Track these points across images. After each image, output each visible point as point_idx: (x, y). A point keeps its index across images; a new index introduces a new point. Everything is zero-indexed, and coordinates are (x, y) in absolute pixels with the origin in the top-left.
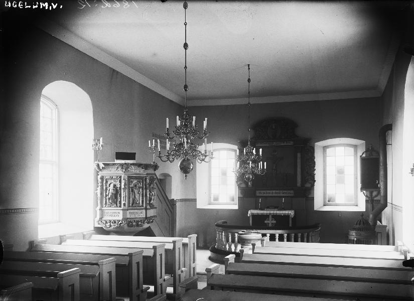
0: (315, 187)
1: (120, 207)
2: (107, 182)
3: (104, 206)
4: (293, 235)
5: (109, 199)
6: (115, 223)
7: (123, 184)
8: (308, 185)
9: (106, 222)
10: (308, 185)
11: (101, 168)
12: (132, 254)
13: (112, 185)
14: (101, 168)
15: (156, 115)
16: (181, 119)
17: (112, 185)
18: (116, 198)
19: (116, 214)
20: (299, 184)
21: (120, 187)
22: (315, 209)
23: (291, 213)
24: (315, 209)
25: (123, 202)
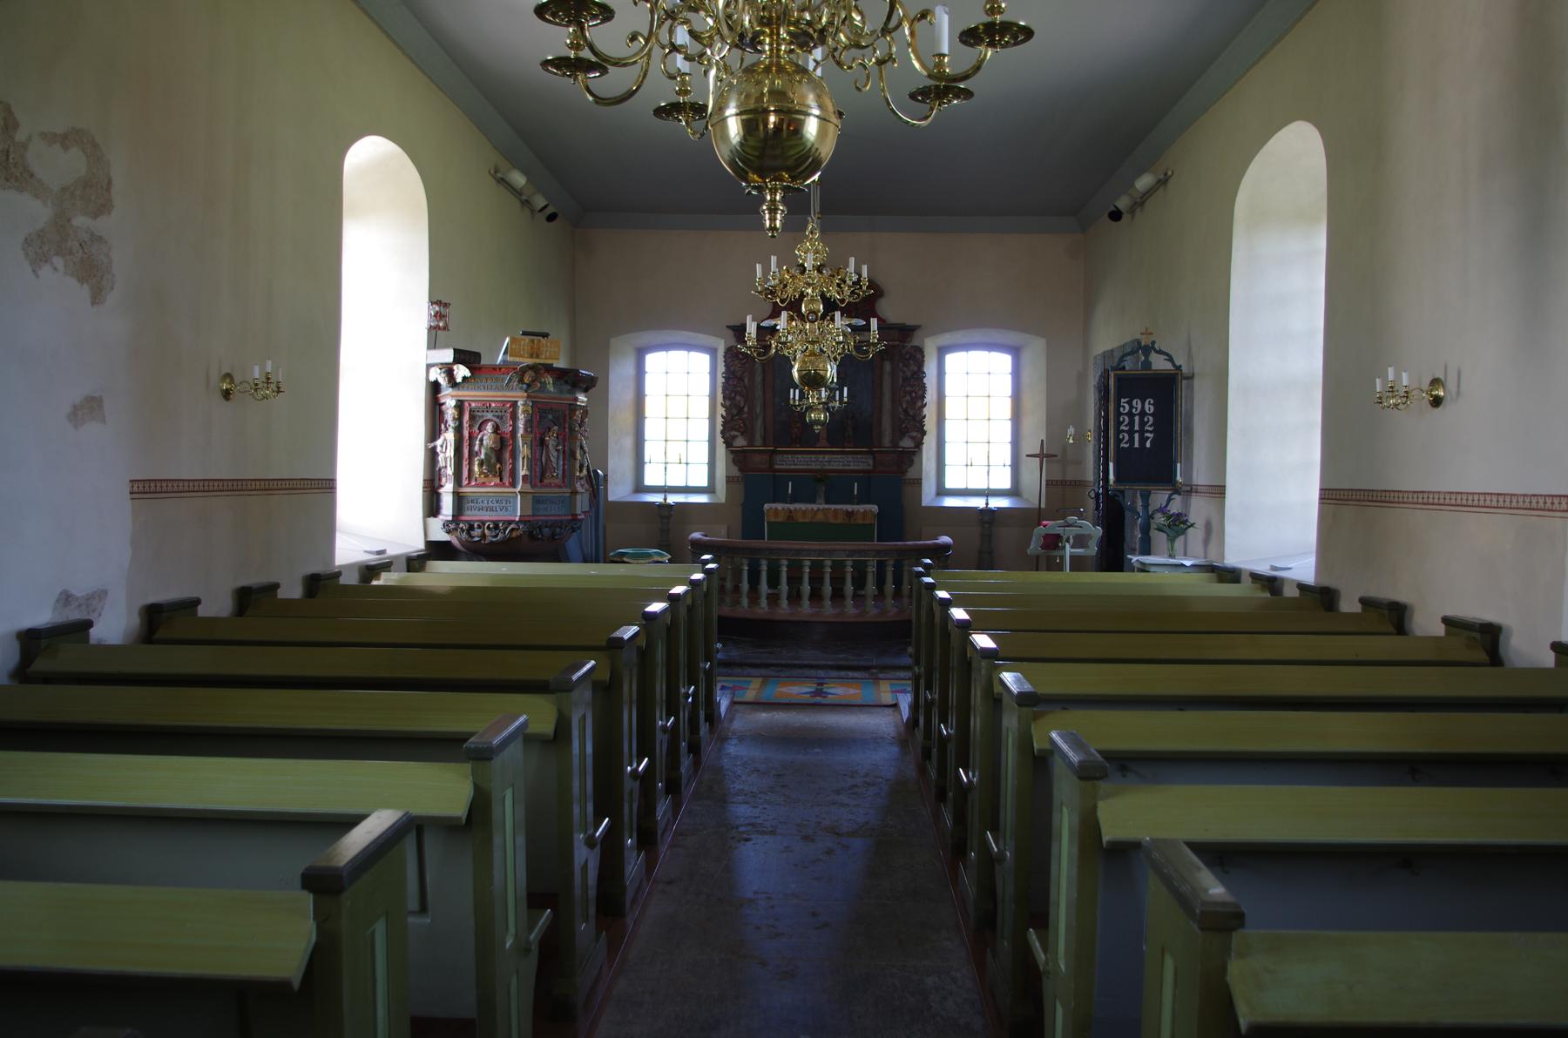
0: (924, 447)
1: (513, 485)
2: (472, 418)
3: (465, 482)
4: (785, 562)
5: (481, 464)
6: (496, 527)
7: (521, 425)
8: (907, 443)
9: (471, 528)
10: (907, 443)
11: (459, 380)
12: (1136, 846)
13: (489, 427)
14: (459, 380)
15: (572, 219)
16: (766, 123)
17: (489, 427)
18: (500, 459)
19: (506, 504)
20: (887, 441)
21: (514, 433)
22: (924, 504)
23: (875, 508)
24: (924, 504)
25: (522, 472)
